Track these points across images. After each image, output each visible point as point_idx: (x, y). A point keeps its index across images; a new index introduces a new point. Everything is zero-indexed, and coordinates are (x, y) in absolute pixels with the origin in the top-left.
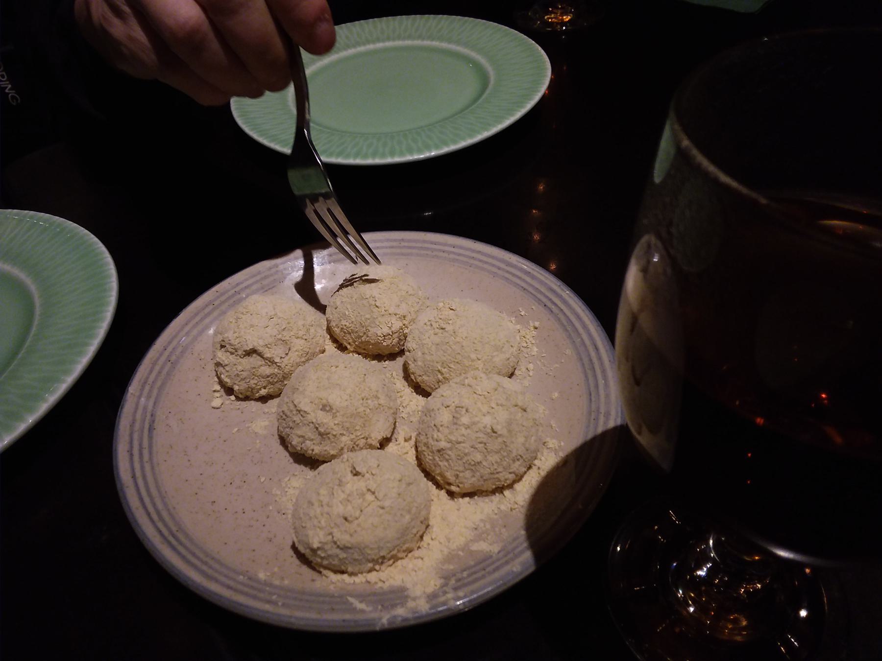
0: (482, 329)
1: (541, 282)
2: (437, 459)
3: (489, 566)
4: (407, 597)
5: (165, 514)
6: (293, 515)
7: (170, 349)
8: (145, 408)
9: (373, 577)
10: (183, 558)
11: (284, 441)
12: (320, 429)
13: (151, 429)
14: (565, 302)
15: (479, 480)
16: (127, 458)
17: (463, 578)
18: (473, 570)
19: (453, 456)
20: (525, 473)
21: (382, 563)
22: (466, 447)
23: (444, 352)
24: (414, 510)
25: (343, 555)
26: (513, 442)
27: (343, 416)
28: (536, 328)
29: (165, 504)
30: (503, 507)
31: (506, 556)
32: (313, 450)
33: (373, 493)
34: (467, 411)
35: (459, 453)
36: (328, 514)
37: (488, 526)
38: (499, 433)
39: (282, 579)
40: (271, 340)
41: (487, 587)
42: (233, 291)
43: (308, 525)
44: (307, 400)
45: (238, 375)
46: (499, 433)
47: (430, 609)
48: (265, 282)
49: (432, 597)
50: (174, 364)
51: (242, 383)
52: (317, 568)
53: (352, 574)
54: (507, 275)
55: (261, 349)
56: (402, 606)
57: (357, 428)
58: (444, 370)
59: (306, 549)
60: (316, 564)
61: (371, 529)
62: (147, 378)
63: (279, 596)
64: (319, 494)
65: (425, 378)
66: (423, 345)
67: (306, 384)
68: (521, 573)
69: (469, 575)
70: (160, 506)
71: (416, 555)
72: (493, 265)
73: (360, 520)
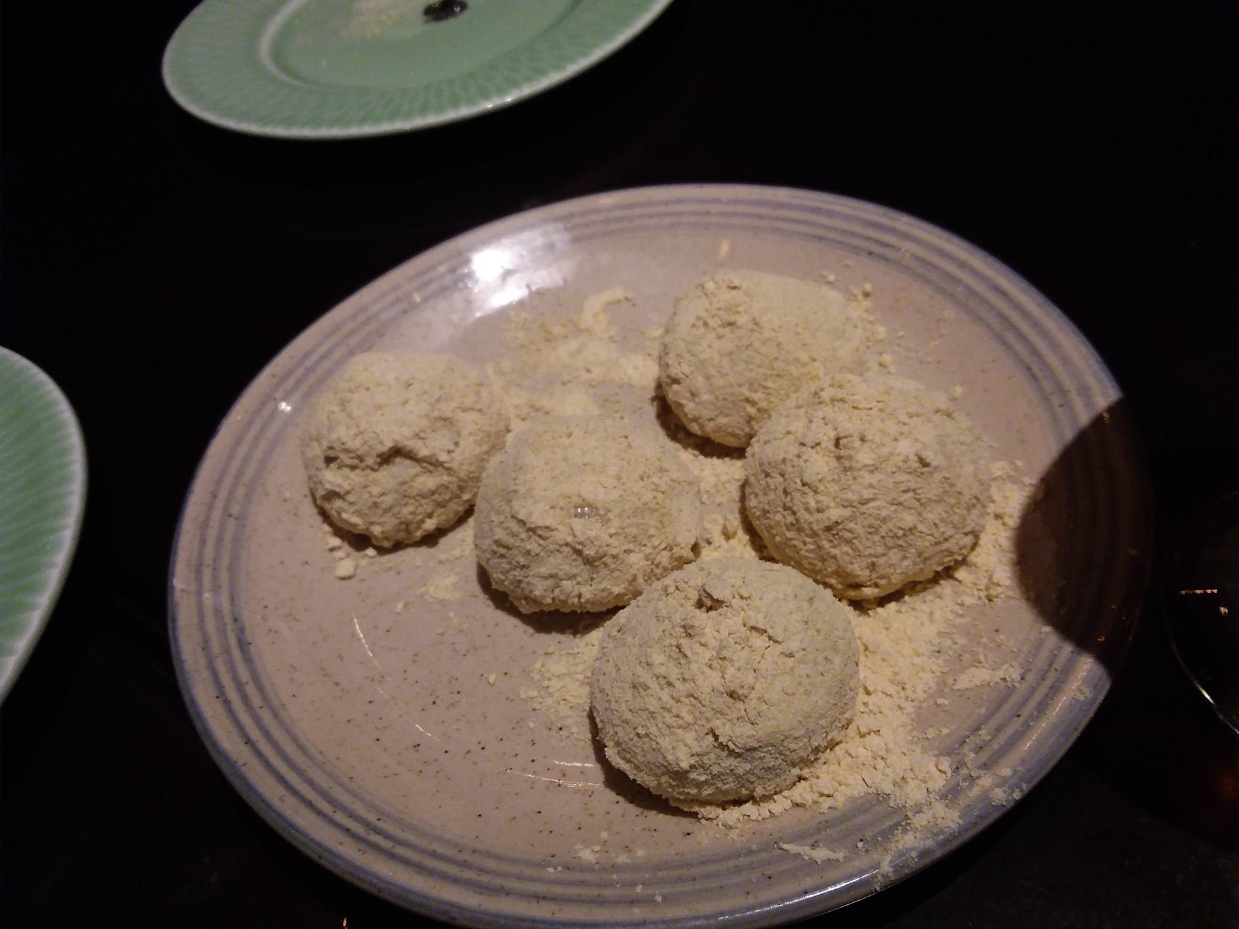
1: (848, 218)
2: (826, 544)
4: (900, 809)
8: (217, 611)
9: (802, 792)
10: (420, 868)
11: (502, 600)
13: (243, 645)
16: (219, 707)
19: (859, 530)
22: (880, 506)
25: (742, 767)
26: (959, 476)
27: (620, 516)
28: (866, 295)
30: (969, 601)
32: (580, 596)
34: (863, 440)
35: (871, 520)
37: (962, 641)
38: (934, 464)
40: (424, 423)
43: (653, 730)
44: (542, 506)
45: (375, 505)
49: (950, 794)
50: (241, 519)
51: (386, 518)
52: (686, 809)
55: (410, 444)
56: (905, 831)
57: (652, 531)
58: (756, 396)
60: (684, 801)
61: (779, 703)
62: (201, 555)
65: (722, 420)
66: (702, 362)
67: (530, 477)
68: (1095, 700)
70: (323, 782)
71: (863, 730)
72: (748, 215)
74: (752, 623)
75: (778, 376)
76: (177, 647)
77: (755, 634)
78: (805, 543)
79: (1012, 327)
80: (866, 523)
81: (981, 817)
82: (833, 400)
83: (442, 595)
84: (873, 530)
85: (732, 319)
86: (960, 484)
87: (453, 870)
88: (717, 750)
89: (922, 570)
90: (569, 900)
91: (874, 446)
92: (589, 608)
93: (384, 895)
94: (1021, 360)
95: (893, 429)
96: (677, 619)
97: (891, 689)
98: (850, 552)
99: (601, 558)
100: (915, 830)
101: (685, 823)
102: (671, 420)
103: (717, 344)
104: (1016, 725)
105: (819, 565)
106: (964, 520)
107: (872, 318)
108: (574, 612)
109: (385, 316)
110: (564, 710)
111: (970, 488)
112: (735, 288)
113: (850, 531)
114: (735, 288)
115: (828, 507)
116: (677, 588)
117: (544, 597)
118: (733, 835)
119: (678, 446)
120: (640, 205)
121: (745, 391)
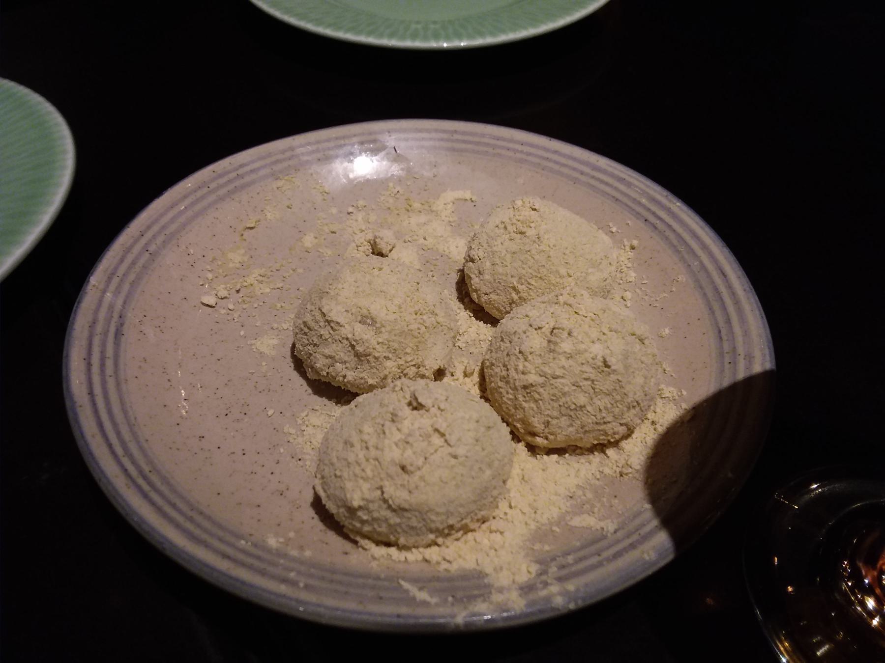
0: (574, 238)
2: (521, 398)
4: (489, 586)
7: (149, 235)
8: (111, 307)
9: (433, 553)
10: (159, 510)
11: (299, 365)
12: (357, 348)
13: (118, 334)
14: (674, 216)
16: (83, 366)
17: (569, 565)
18: (581, 554)
19: (546, 396)
21: (449, 535)
22: (565, 384)
24: (496, 463)
25: (395, 520)
26: (629, 383)
27: (390, 332)
28: (633, 248)
30: (607, 471)
31: (628, 536)
32: (345, 377)
33: (443, 435)
34: (569, 334)
35: (555, 391)
36: (377, 459)
37: (590, 495)
38: (613, 367)
39: (302, 548)
42: (233, 175)
43: (345, 475)
47: (527, 606)
48: (279, 167)
49: (527, 589)
50: (154, 256)
52: (352, 537)
53: (401, 548)
54: (593, 182)
56: (484, 601)
57: (408, 350)
58: (520, 287)
59: (338, 507)
60: (351, 531)
61: (436, 485)
62: (116, 268)
63: (299, 573)
64: (361, 431)
65: (493, 297)
66: (493, 253)
67: (340, 286)
70: (127, 436)
71: (493, 528)
72: (575, 169)
73: (424, 469)
74: (437, 426)
75: (540, 278)
76: (74, 319)
77: (437, 435)
78: (508, 393)
80: (552, 392)
81: (540, 611)
82: (565, 303)
83: (264, 349)
84: (555, 398)
85: (524, 230)
86: (628, 388)
87: (180, 519)
88: (381, 502)
90: (243, 565)
91: (575, 341)
92: (349, 387)
94: (717, 323)
95: (594, 334)
96: (391, 409)
97: (527, 510)
98: (535, 408)
100: (491, 603)
101: (348, 546)
102: (464, 291)
103: (507, 243)
104: (594, 560)
107: (630, 265)
109: (305, 158)
110: (308, 448)
112: (535, 210)
113: (539, 394)
114: (535, 210)
115: (530, 373)
116: (402, 389)
117: (322, 370)
118: (374, 564)
119: (462, 306)
120: (504, 139)
121: (515, 281)
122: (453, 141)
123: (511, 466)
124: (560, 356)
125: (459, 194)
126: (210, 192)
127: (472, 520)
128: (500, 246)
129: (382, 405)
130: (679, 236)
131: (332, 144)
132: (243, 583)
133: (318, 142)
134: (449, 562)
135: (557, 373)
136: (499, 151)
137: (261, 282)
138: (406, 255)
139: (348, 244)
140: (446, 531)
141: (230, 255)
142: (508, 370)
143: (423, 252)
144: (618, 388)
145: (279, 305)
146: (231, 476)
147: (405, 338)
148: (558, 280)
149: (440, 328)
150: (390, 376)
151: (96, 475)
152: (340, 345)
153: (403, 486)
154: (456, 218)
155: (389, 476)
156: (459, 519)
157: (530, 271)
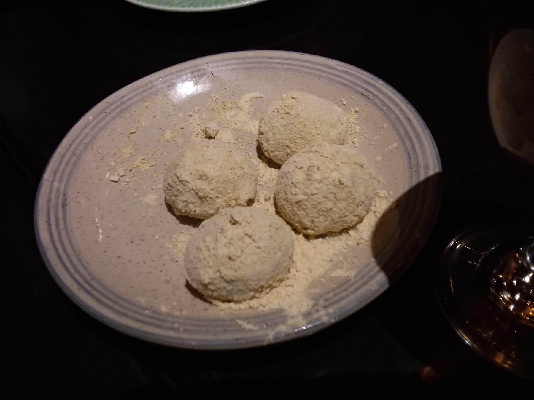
1: (357, 77)
2: (296, 209)
3: (349, 287)
4: (286, 316)
5: (80, 267)
6: (185, 260)
7: (74, 146)
8: (58, 190)
9: (254, 303)
11: (170, 208)
12: (200, 194)
13: (64, 205)
15: (330, 224)
18: (336, 291)
19: (309, 206)
20: (366, 215)
21: (261, 291)
22: (319, 198)
23: (291, 131)
24: (284, 248)
27: (217, 182)
28: (356, 112)
29: (80, 260)
30: (350, 243)
31: (362, 278)
32: (195, 211)
33: (250, 237)
34: (318, 169)
35: (314, 202)
36: (214, 255)
37: (341, 258)
38: (345, 184)
39: (181, 310)
41: (352, 302)
43: (199, 266)
44: (187, 173)
46: (345, 184)
48: (144, 95)
49: (307, 315)
50: (79, 157)
52: (208, 300)
53: (237, 302)
54: (330, 76)
57: (229, 191)
58: (291, 145)
59: (198, 284)
61: (250, 264)
63: (180, 324)
64: (205, 241)
65: (277, 153)
66: (273, 127)
67: (185, 160)
68: (378, 291)
69: (334, 296)
70: (75, 261)
71: (287, 284)
72: (318, 70)
74: (247, 232)
75: (302, 138)
77: (247, 237)
78: (288, 207)
79: (409, 135)
82: (316, 151)
83: (149, 202)
85: (289, 111)
87: (111, 304)
88: (221, 279)
89: (333, 227)
93: (82, 307)
96: (220, 226)
97: (306, 271)
98: (304, 214)
99: (206, 197)
101: (207, 305)
102: (260, 152)
103: (280, 120)
105: (293, 217)
106: (355, 210)
107: (356, 122)
108: (194, 218)
109: (160, 86)
111: (360, 197)
112: (294, 98)
113: (305, 205)
114: (294, 98)
115: (299, 194)
119: (260, 161)
120: (276, 58)
121: (287, 142)
122: (245, 63)
123: (293, 248)
124: (314, 182)
125: (253, 95)
126: (106, 116)
127: (274, 281)
128: (276, 123)
129: (215, 225)
130: (382, 101)
131: (174, 76)
132: (148, 333)
133: (166, 76)
134: (264, 306)
135: (314, 192)
136: (273, 65)
137: (143, 163)
138: (225, 136)
139: (191, 134)
140: (260, 290)
141: (124, 150)
142: (287, 194)
143: (236, 132)
144: (350, 195)
145: (155, 175)
146: (138, 276)
147: (226, 185)
148: (312, 138)
149: (247, 176)
150: (221, 207)
151: (61, 286)
152: (190, 194)
153: (231, 268)
154: (252, 109)
155: (223, 264)
156: (266, 282)
157: (295, 135)
